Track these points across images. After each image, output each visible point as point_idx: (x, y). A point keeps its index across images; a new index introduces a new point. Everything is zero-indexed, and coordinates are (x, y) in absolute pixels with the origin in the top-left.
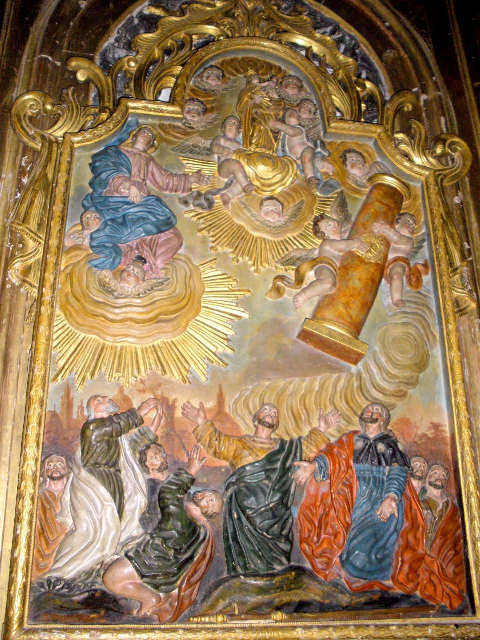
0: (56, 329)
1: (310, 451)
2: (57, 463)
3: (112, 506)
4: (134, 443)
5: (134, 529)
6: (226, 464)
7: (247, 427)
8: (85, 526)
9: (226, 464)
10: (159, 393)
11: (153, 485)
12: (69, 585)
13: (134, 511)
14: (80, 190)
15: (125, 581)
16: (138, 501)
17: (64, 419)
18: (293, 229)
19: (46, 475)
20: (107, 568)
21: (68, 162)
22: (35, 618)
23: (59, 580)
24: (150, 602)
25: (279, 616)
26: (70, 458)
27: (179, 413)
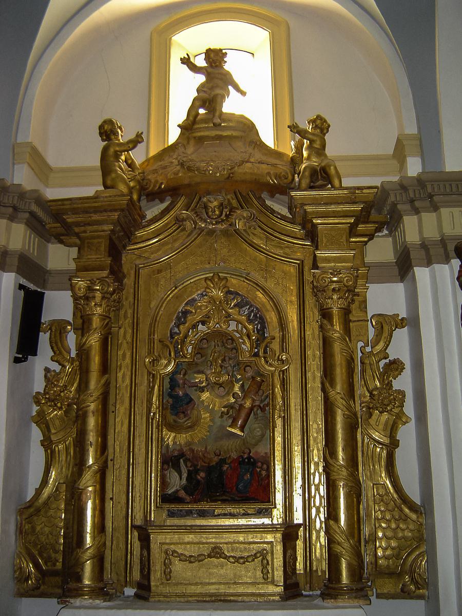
0: (45, 220)
1: (228, 461)
2: (166, 466)
3: (178, 478)
4: (183, 460)
5: (184, 481)
6: (207, 465)
7: (212, 456)
8: (172, 481)
9: (207, 465)
10: (190, 446)
11: (189, 471)
12: (169, 495)
13: (184, 478)
14: (167, 390)
15: (182, 494)
16: (185, 475)
17: (167, 455)
18: (398, 224)
19: (162, 469)
20: (177, 491)
21: (189, 563)
22: (162, 502)
23: (167, 494)
24: (188, 498)
25: (219, 502)
26: (169, 465)
27: (195, 452)
